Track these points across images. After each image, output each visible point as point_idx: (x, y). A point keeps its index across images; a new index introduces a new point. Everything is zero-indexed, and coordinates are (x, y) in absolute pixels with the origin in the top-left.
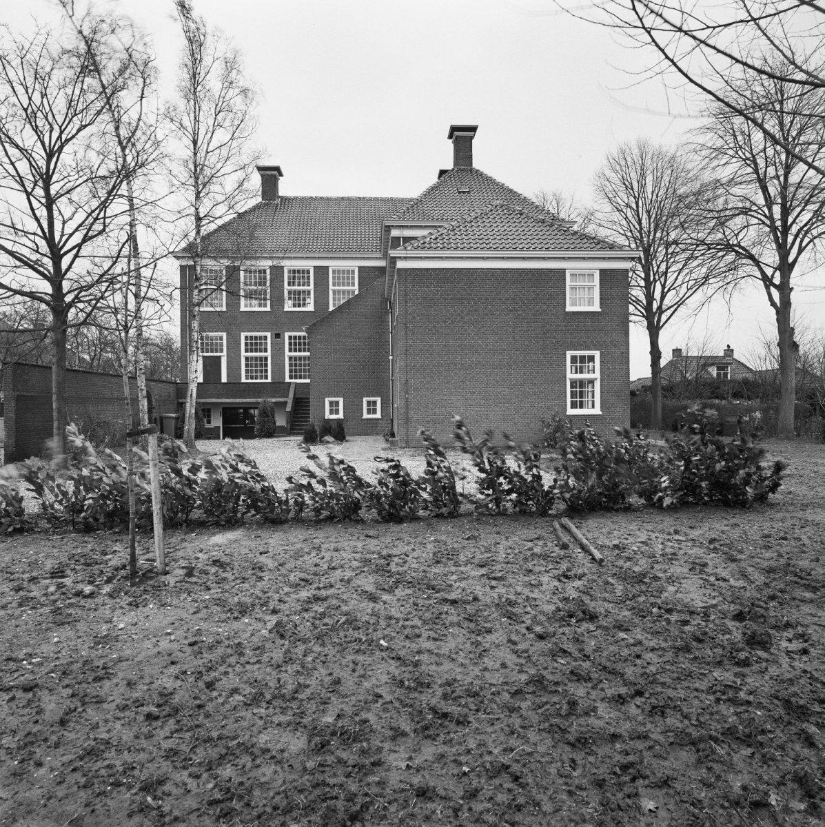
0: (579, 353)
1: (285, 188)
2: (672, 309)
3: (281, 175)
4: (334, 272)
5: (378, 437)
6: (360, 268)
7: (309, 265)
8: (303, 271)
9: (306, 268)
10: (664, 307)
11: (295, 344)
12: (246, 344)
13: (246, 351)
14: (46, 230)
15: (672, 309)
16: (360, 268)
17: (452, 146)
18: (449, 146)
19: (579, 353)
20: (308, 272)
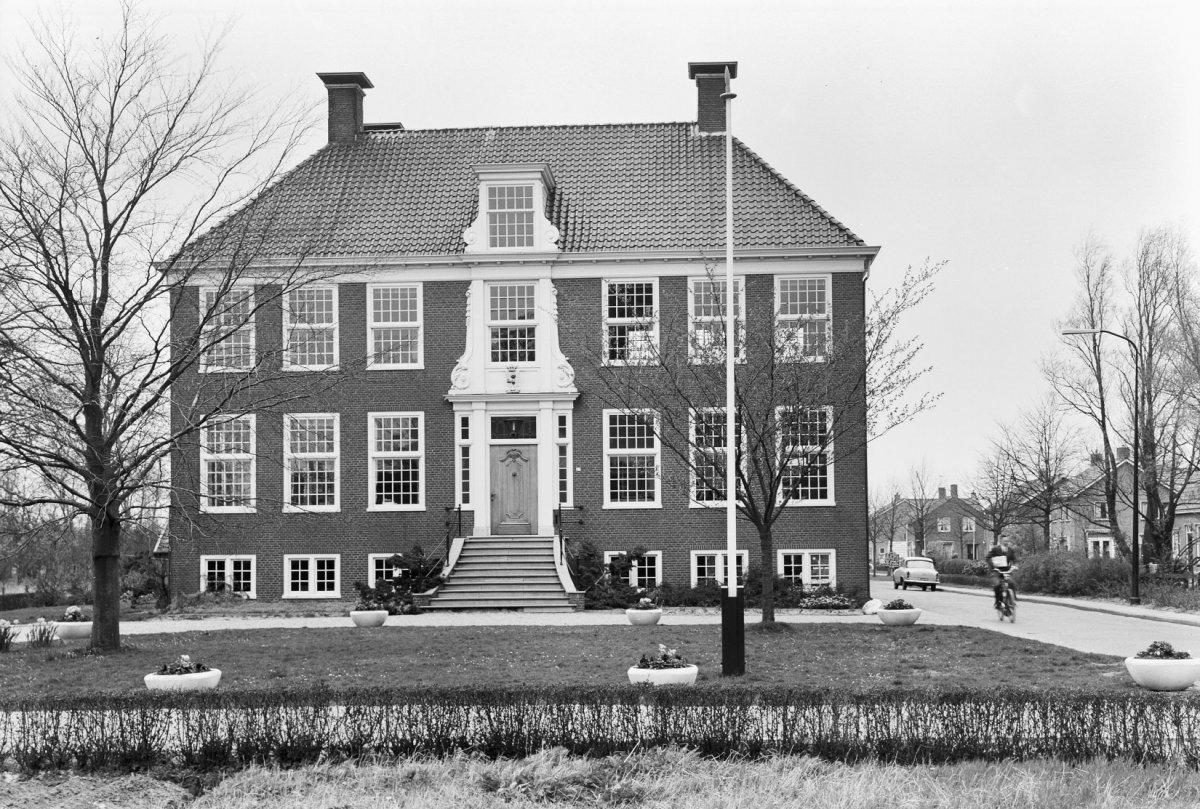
0: (818, 502)
1: (374, 110)
2: (196, 225)
3: (367, 84)
4: (612, 288)
5: (759, 610)
6: (426, 284)
7: (649, 275)
8: (639, 288)
9: (644, 281)
10: (111, 221)
11: (622, 431)
12: (613, 432)
13: (613, 445)
14: (63, 296)
15: (125, 215)
16: (426, 284)
17: (696, 90)
18: (691, 90)
19: (818, 502)
20: (649, 288)
